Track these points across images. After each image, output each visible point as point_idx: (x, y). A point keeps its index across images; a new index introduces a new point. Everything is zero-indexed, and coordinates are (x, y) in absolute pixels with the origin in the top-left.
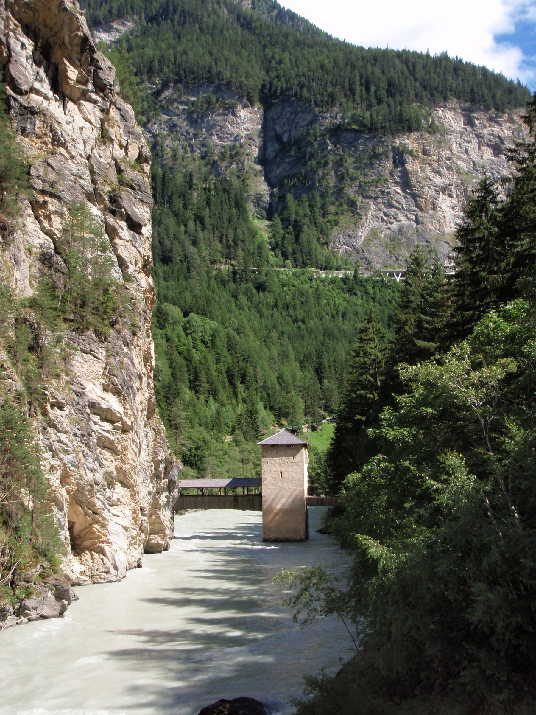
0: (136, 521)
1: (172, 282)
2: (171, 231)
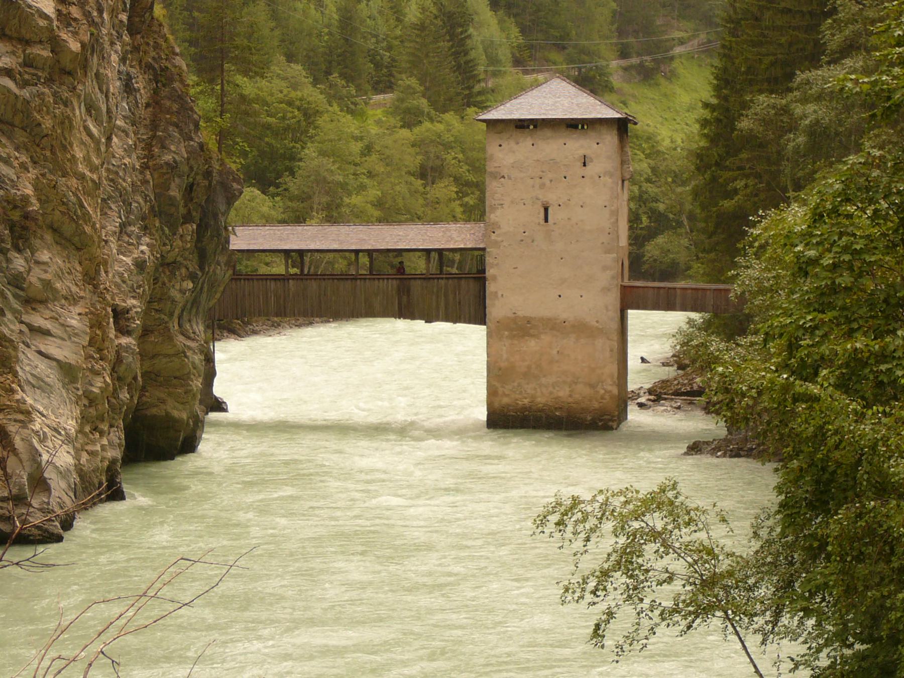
0: (100, 350)
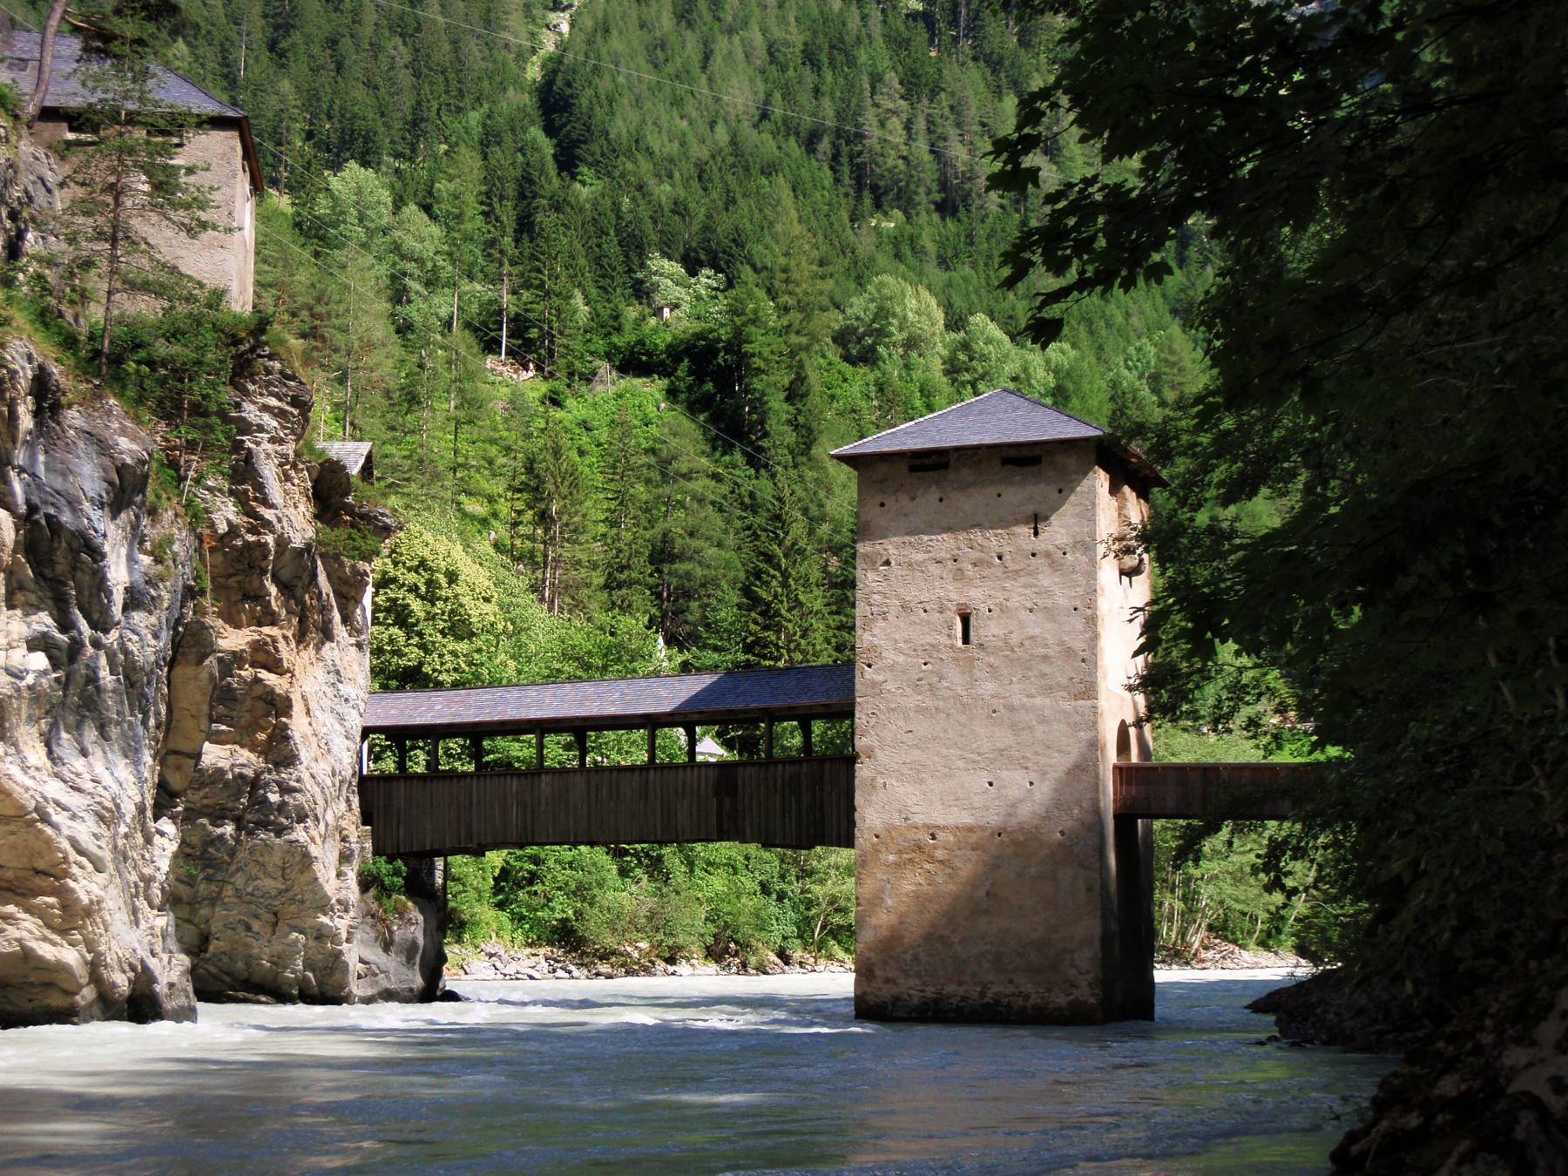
1: (967, 270)
2: (972, 113)
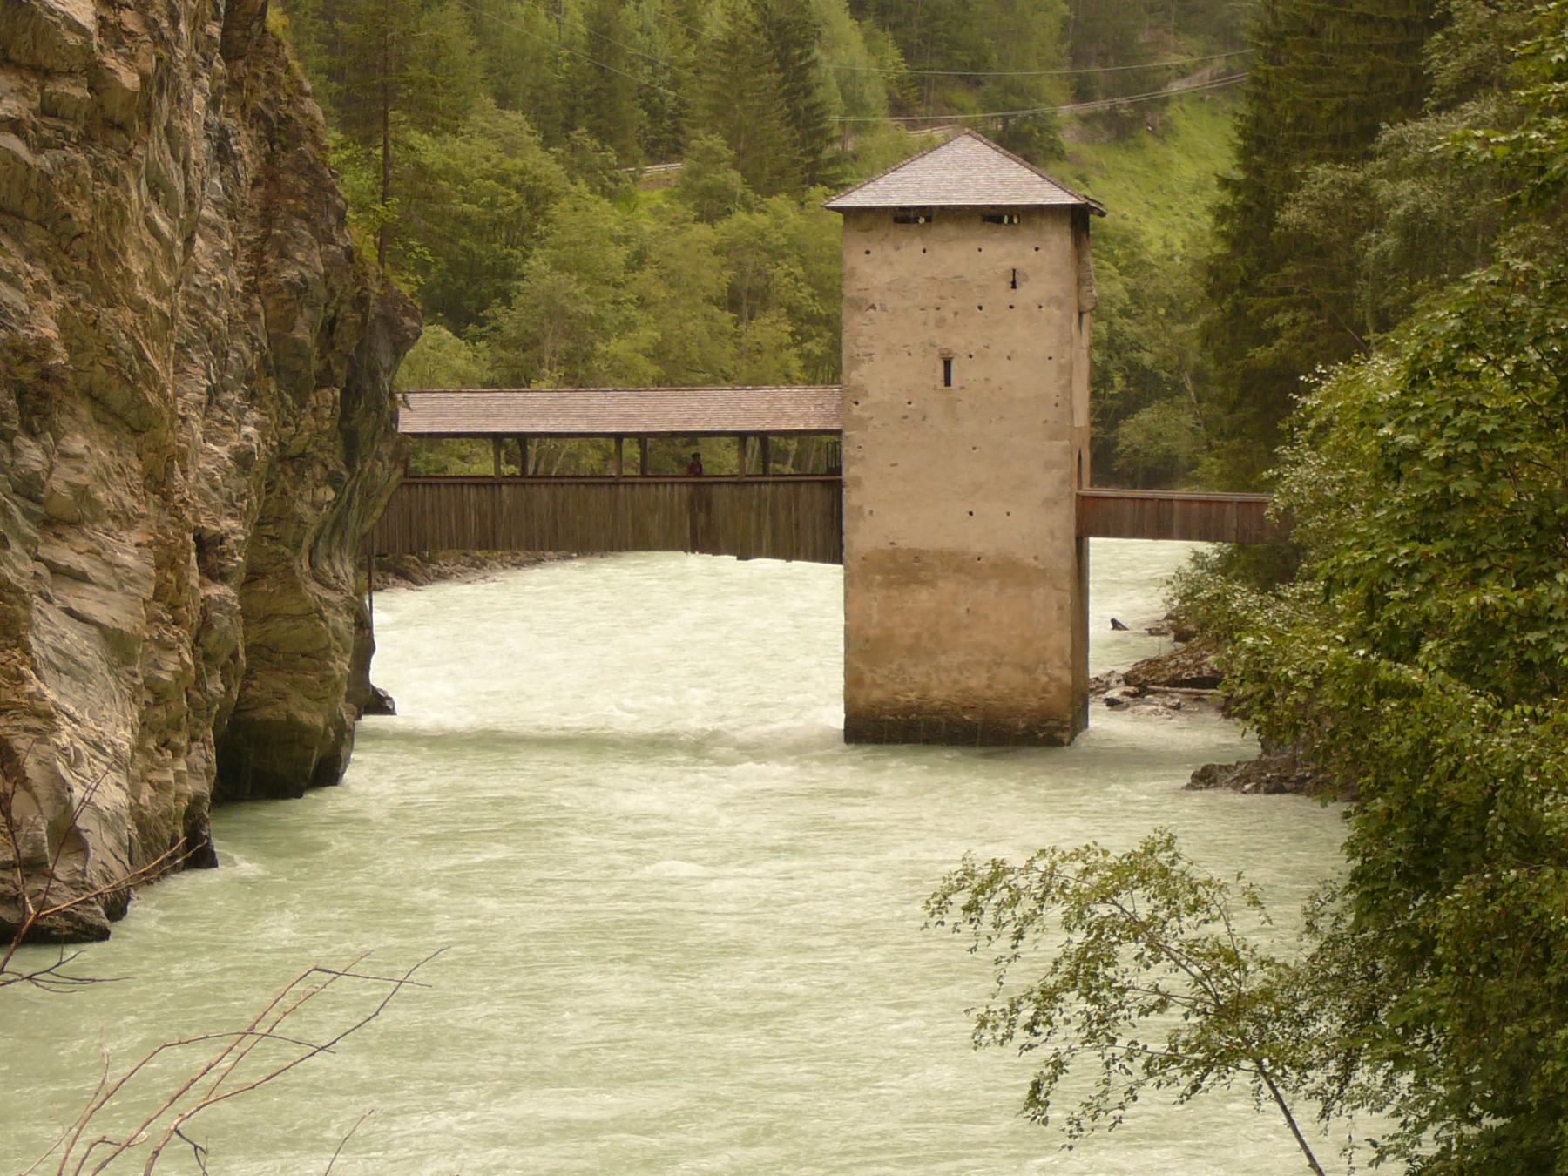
0: (173, 607)
